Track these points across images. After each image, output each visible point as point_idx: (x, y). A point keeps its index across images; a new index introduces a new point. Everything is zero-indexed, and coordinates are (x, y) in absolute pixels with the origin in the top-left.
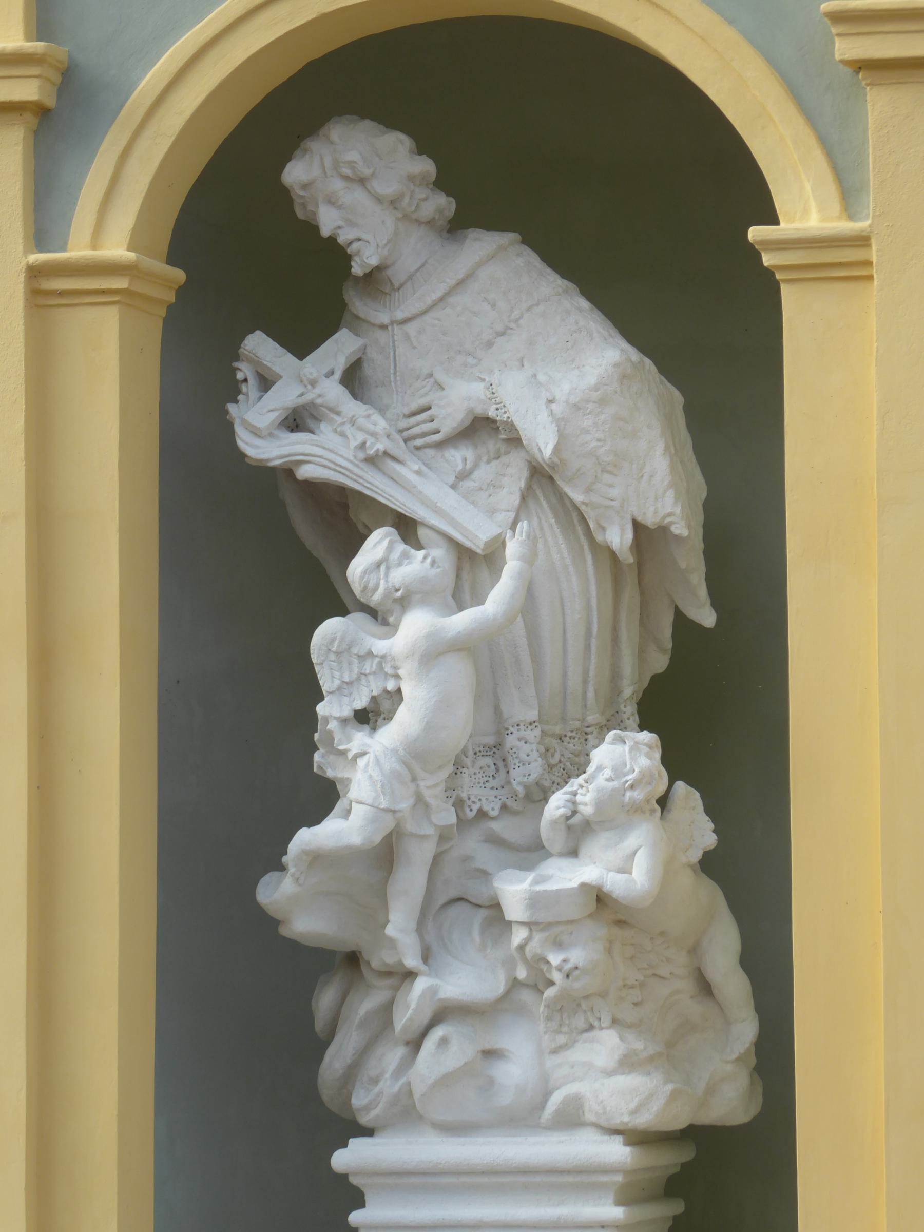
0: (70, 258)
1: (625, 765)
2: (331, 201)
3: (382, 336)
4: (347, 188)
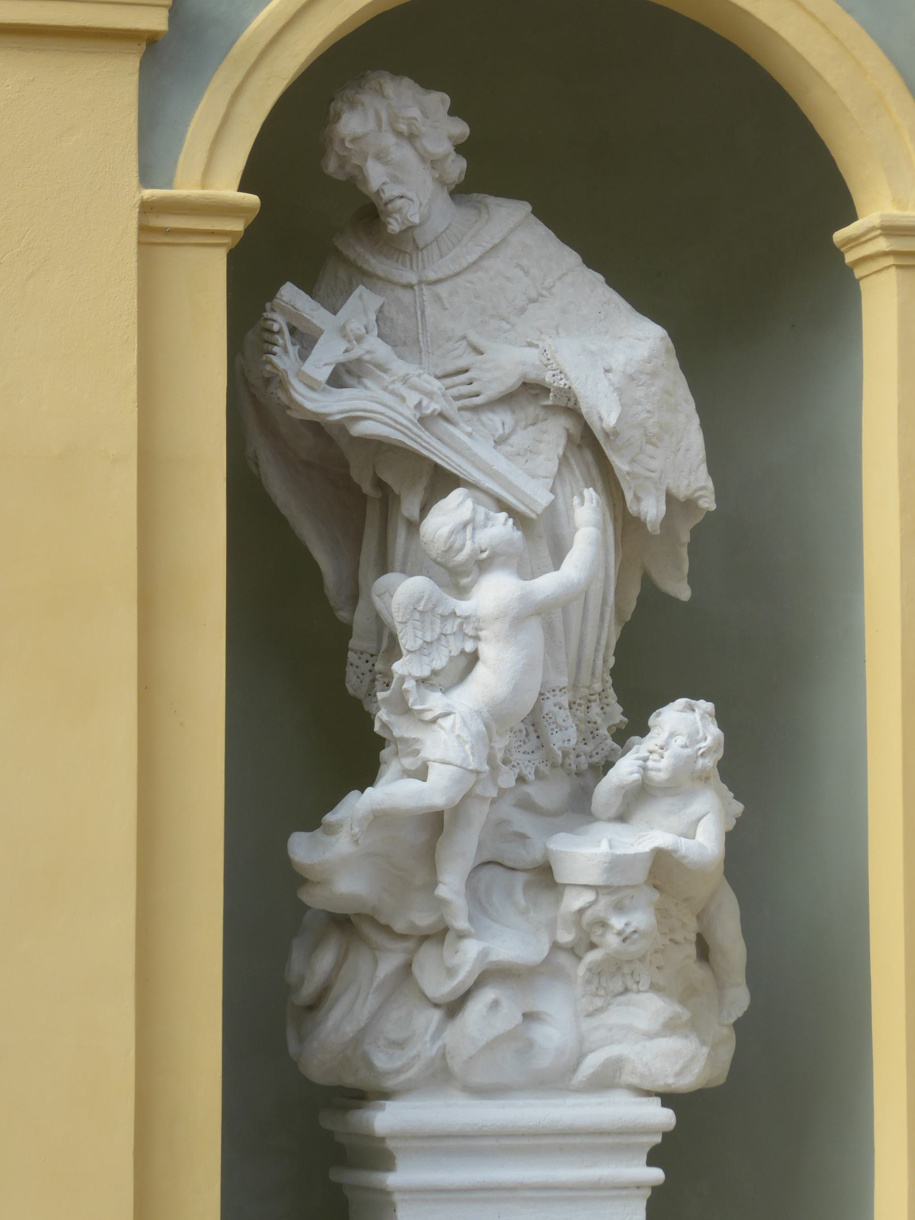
0: (188, 196)
1: (698, 732)
2: (381, 157)
3: (406, 297)
4: (397, 144)
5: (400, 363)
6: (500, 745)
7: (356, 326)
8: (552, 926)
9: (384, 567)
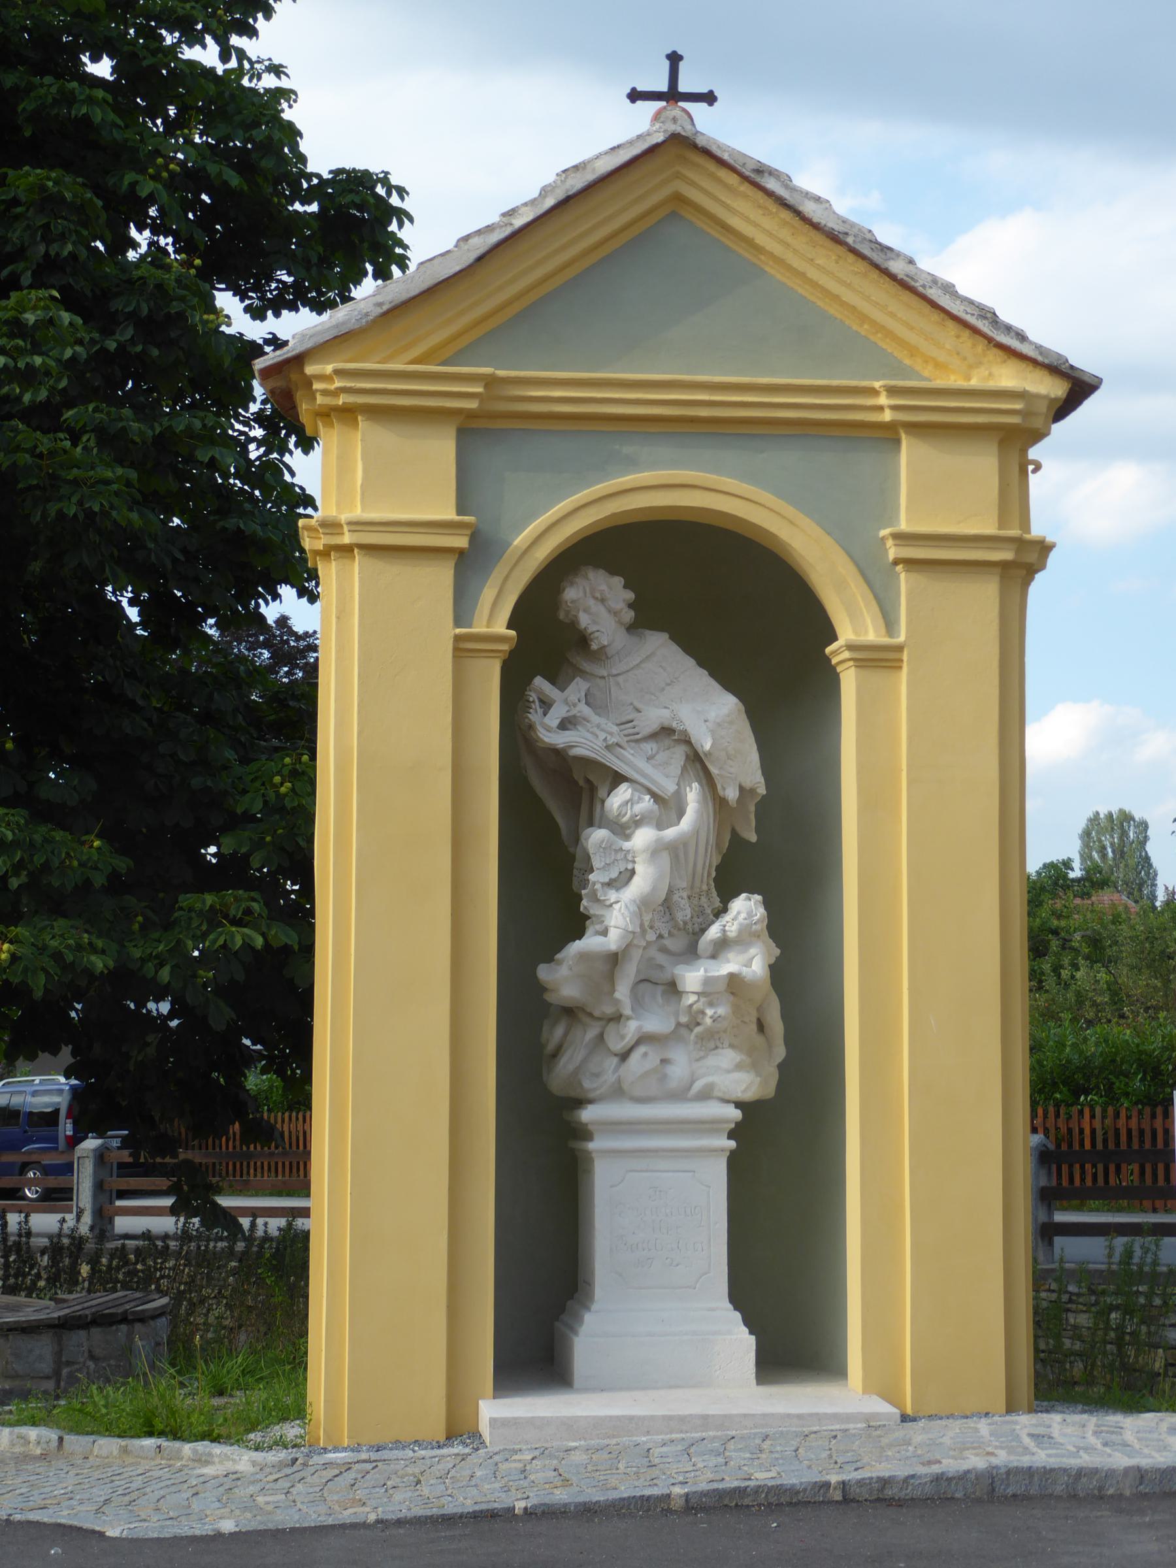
3: (601, 682)
5: (597, 717)
6: (647, 918)
7: (573, 698)
8: (677, 1014)
9: (591, 823)
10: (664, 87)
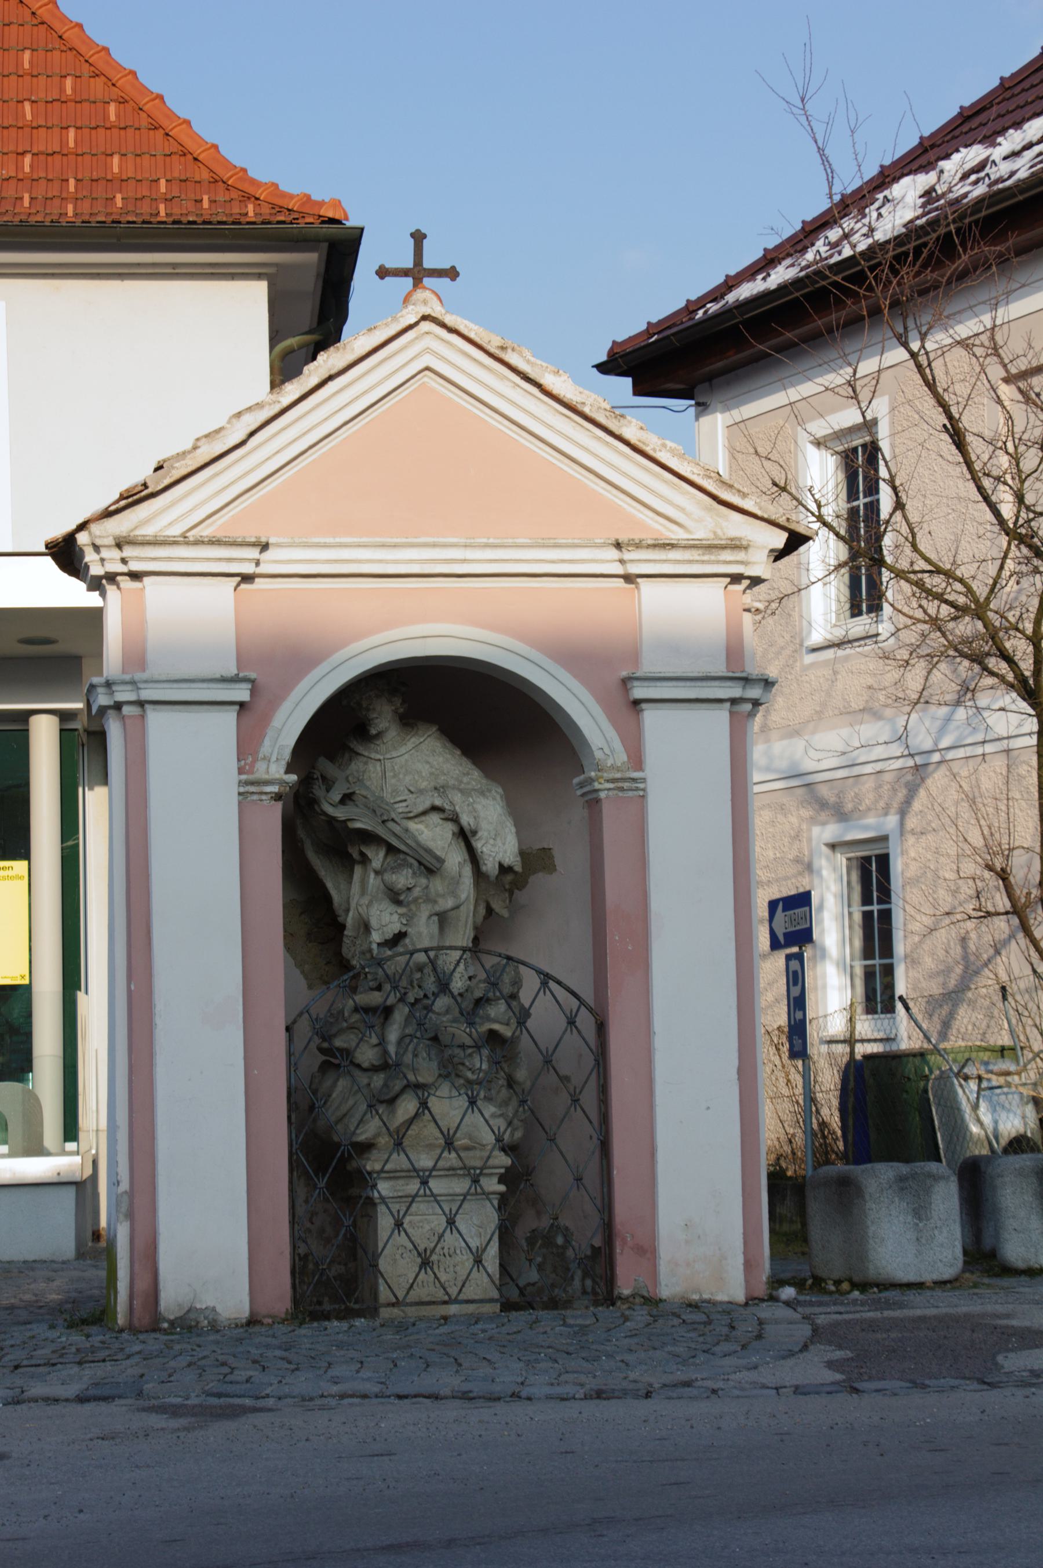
10: (409, 263)
